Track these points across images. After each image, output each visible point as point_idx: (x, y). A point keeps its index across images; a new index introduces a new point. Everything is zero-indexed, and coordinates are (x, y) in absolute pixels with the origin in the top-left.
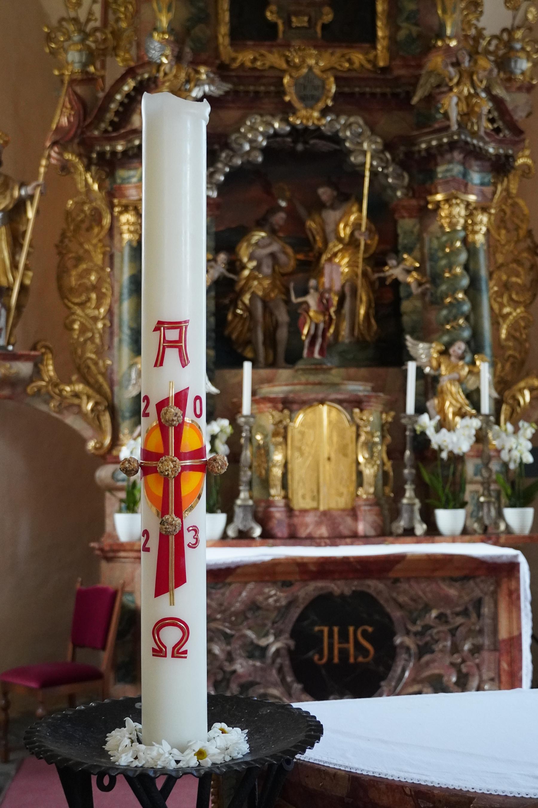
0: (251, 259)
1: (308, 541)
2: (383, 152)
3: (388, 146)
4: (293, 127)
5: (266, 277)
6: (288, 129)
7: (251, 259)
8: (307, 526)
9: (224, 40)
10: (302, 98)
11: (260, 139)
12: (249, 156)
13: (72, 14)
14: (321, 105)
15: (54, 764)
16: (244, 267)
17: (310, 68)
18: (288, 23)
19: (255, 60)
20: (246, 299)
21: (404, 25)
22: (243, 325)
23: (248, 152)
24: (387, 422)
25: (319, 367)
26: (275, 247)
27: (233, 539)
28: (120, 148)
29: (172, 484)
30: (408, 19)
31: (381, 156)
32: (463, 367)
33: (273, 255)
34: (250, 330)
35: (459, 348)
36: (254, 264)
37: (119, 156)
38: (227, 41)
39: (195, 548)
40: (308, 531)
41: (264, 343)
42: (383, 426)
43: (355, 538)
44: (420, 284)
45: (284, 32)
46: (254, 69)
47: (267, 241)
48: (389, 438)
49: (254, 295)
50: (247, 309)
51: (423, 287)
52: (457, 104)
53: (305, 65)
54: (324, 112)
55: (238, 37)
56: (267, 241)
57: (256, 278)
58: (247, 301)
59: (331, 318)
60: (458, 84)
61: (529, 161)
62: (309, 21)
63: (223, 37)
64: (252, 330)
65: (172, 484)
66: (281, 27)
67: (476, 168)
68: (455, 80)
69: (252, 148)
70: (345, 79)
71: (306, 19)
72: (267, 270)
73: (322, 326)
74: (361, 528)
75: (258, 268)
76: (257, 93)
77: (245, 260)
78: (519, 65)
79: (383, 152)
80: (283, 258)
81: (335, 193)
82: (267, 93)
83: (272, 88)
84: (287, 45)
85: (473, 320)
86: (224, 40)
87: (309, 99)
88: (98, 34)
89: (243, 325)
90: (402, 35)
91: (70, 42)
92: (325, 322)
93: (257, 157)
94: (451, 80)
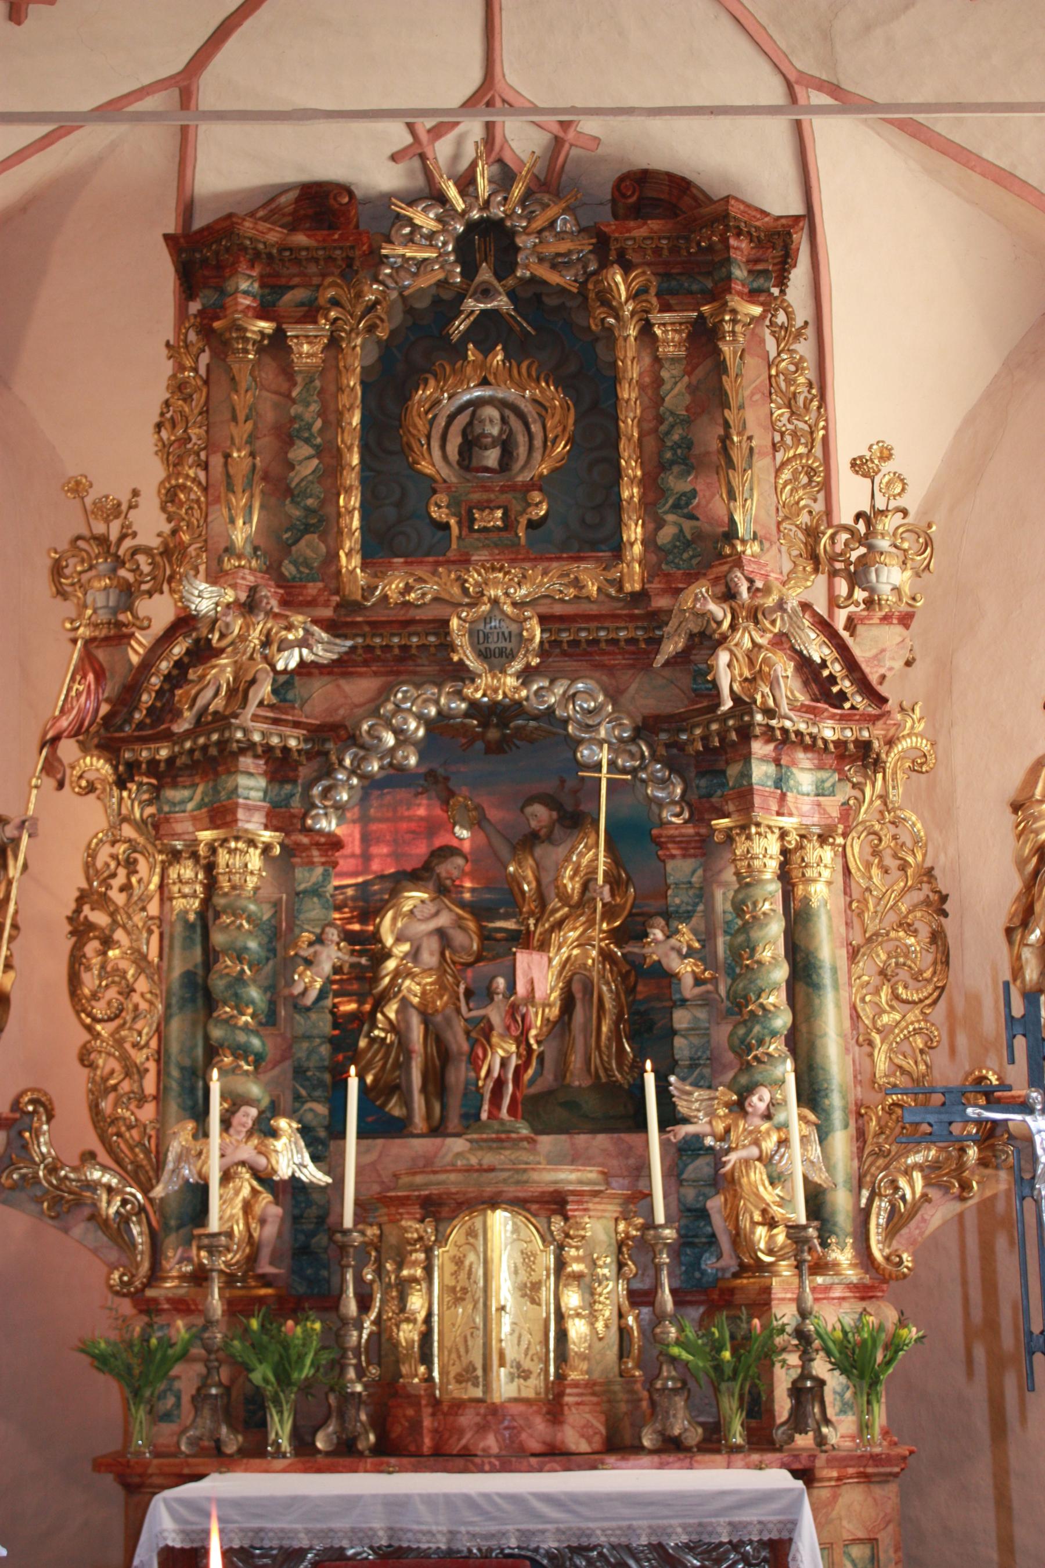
0: (399, 940)
1: (460, 1462)
2: (633, 740)
3: (646, 728)
4: (473, 704)
5: (427, 971)
6: (463, 706)
7: (399, 940)
8: (461, 1432)
9: (350, 562)
10: (484, 655)
11: (413, 725)
12: (393, 757)
13: (99, 528)
14: (517, 666)
16: (388, 955)
17: (495, 602)
18: (467, 521)
19: (408, 589)
20: (391, 1011)
21: (670, 518)
22: (386, 1057)
23: (392, 750)
24: (628, 1237)
25: (503, 1136)
26: (444, 920)
27: (328, 1454)
28: (164, 753)
29: (645, 1299)
30: (676, 507)
31: (634, 748)
32: (768, 1133)
33: (441, 933)
34: (397, 1065)
35: (761, 1099)
36: (406, 947)
37: (162, 766)
38: (356, 561)
40: (463, 1442)
41: (424, 1089)
42: (620, 1245)
43: (556, 1456)
44: (698, 981)
45: (459, 538)
46: (407, 604)
48: (631, 1267)
49: (405, 1003)
50: (392, 1028)
51: (703, 988)
52: (729, 665)
53: (485, 599)
54: (527, 675)
55: (378, 547)
56: (431, 908)
57: (410, 974)
58: (392, 1016)
59: (529, 1049)
60: (733, 627)
61: (924, 745)
62: (505, 517)
63: (348, 555)
64: (403, 1066)
65: (645, 1299)
66: (455, 530)
67: (807, 764)
68: (726, 624)
69: (399, 743)
70: (561, 618)
71: (499, 514)
72: (429, 958)
73: (514, 1062)
74: (572, 1438)
75: (415, 955)
76: (405, 648)
77: (389, 941)
78: (883, 578)
79: (633, 740)
80: (459, 938)
81: (555, 814)
82: (423, 647)
83: (432, 639)
84: (464, 562)
85: (801, 1043)
86: (350, 562)
87: (496, 658)
89: (386, 1057)
90: (666, 535)
91: (93, 573)
92: (519, 1056)
93: (406, 758)
94: (719, 623)
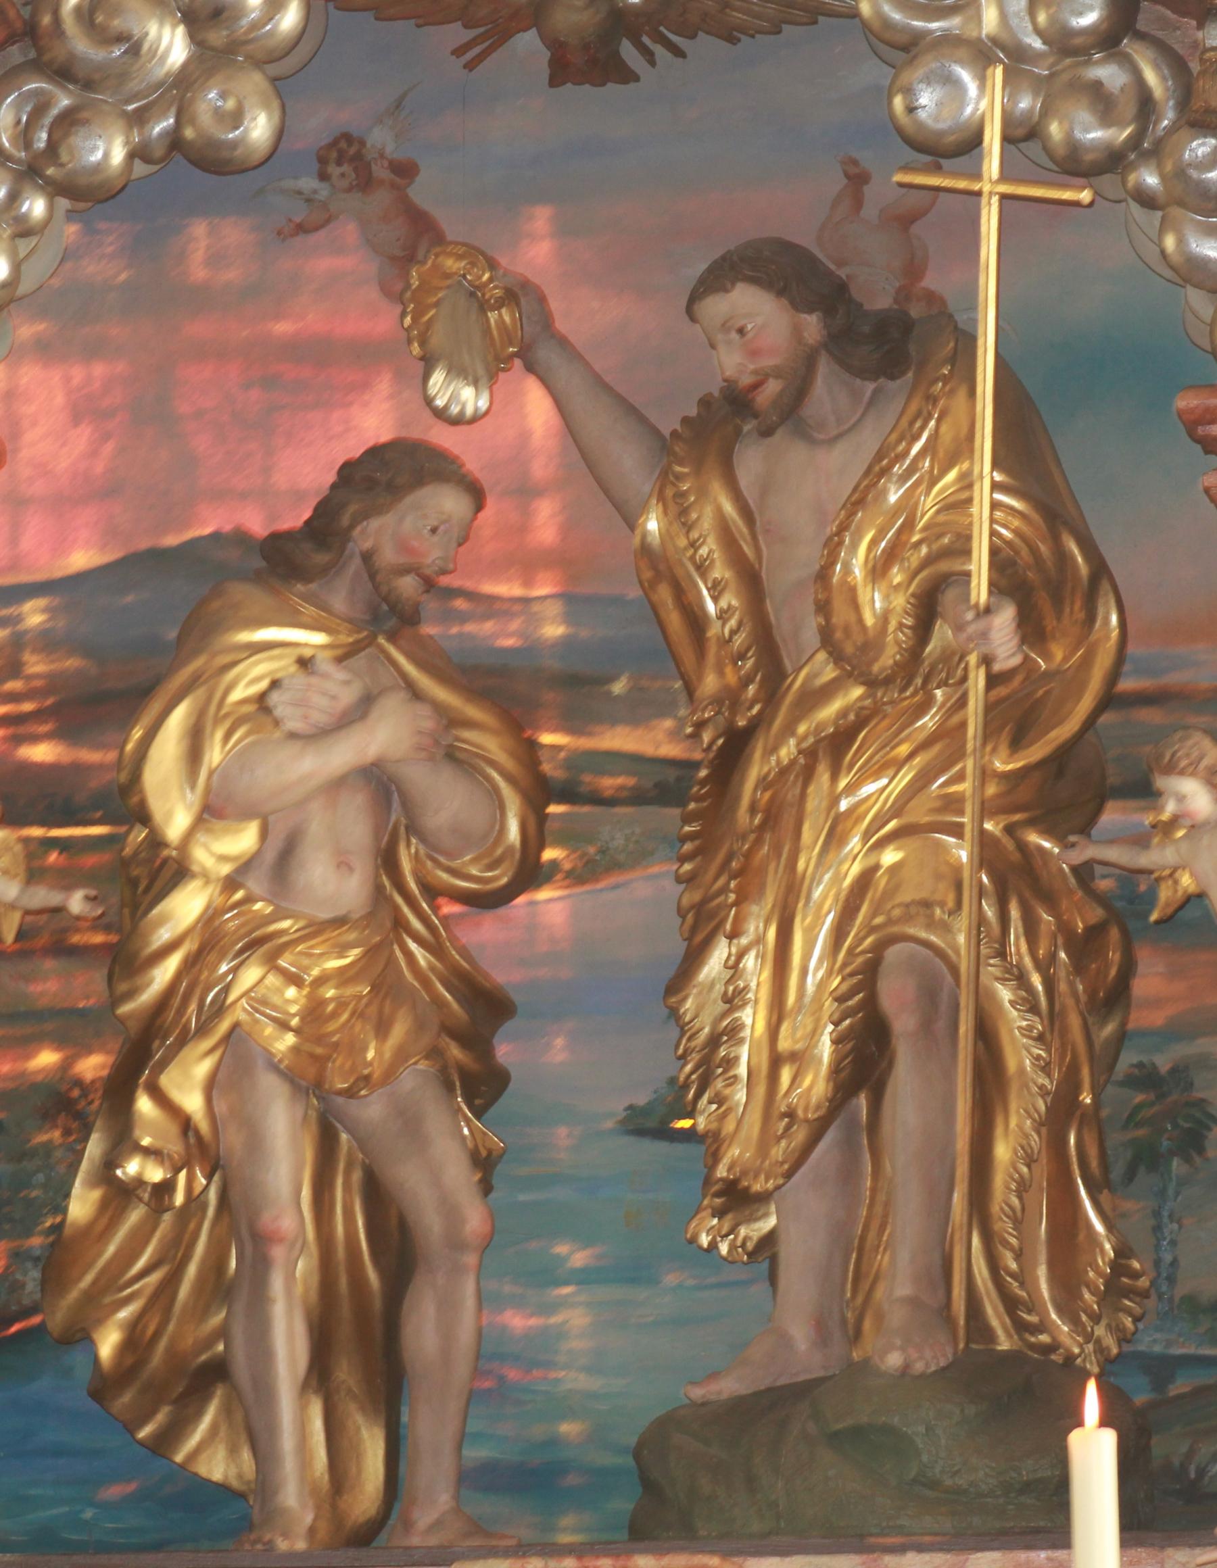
0: (213, 812)
7: (213, 812)
15: (700, 33)
16: (170, 871)
20: (188, 1082)
23: (184, 83)
26: (388, 734)
33: (380, 783)
34: (216, 1286)
36: (243, 840)
39: (509, 370)
41: (319, 1374)
47: (338, 688)
50: (197, 1147)
64: (236, 1287)
72: (333, 881)
75: (280, 861)
77: (176, 818)
80: (446, 801)
88: (385, 607)
